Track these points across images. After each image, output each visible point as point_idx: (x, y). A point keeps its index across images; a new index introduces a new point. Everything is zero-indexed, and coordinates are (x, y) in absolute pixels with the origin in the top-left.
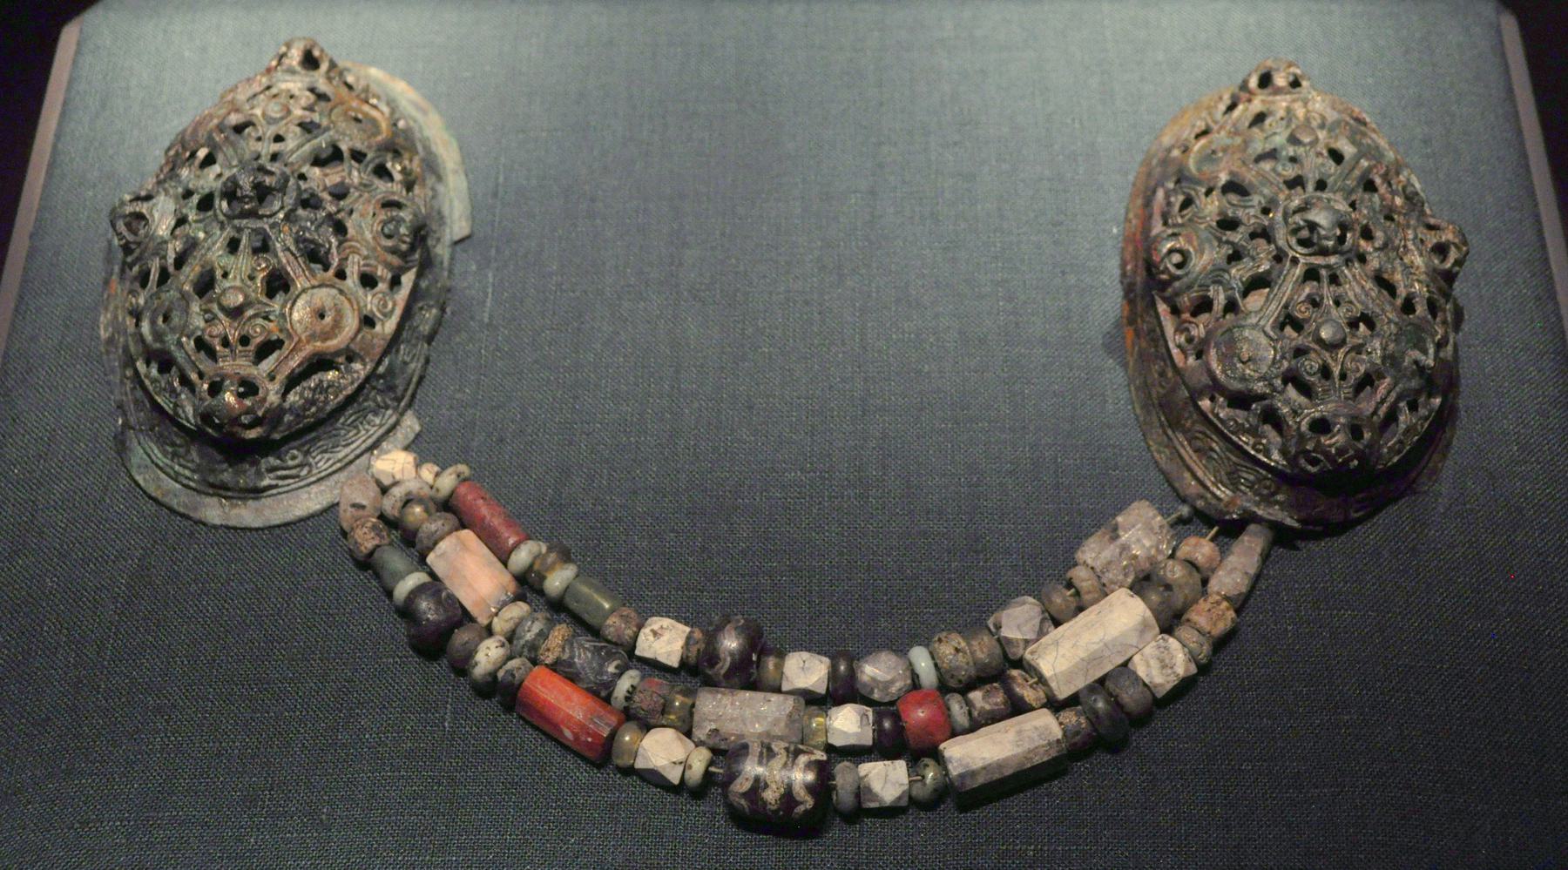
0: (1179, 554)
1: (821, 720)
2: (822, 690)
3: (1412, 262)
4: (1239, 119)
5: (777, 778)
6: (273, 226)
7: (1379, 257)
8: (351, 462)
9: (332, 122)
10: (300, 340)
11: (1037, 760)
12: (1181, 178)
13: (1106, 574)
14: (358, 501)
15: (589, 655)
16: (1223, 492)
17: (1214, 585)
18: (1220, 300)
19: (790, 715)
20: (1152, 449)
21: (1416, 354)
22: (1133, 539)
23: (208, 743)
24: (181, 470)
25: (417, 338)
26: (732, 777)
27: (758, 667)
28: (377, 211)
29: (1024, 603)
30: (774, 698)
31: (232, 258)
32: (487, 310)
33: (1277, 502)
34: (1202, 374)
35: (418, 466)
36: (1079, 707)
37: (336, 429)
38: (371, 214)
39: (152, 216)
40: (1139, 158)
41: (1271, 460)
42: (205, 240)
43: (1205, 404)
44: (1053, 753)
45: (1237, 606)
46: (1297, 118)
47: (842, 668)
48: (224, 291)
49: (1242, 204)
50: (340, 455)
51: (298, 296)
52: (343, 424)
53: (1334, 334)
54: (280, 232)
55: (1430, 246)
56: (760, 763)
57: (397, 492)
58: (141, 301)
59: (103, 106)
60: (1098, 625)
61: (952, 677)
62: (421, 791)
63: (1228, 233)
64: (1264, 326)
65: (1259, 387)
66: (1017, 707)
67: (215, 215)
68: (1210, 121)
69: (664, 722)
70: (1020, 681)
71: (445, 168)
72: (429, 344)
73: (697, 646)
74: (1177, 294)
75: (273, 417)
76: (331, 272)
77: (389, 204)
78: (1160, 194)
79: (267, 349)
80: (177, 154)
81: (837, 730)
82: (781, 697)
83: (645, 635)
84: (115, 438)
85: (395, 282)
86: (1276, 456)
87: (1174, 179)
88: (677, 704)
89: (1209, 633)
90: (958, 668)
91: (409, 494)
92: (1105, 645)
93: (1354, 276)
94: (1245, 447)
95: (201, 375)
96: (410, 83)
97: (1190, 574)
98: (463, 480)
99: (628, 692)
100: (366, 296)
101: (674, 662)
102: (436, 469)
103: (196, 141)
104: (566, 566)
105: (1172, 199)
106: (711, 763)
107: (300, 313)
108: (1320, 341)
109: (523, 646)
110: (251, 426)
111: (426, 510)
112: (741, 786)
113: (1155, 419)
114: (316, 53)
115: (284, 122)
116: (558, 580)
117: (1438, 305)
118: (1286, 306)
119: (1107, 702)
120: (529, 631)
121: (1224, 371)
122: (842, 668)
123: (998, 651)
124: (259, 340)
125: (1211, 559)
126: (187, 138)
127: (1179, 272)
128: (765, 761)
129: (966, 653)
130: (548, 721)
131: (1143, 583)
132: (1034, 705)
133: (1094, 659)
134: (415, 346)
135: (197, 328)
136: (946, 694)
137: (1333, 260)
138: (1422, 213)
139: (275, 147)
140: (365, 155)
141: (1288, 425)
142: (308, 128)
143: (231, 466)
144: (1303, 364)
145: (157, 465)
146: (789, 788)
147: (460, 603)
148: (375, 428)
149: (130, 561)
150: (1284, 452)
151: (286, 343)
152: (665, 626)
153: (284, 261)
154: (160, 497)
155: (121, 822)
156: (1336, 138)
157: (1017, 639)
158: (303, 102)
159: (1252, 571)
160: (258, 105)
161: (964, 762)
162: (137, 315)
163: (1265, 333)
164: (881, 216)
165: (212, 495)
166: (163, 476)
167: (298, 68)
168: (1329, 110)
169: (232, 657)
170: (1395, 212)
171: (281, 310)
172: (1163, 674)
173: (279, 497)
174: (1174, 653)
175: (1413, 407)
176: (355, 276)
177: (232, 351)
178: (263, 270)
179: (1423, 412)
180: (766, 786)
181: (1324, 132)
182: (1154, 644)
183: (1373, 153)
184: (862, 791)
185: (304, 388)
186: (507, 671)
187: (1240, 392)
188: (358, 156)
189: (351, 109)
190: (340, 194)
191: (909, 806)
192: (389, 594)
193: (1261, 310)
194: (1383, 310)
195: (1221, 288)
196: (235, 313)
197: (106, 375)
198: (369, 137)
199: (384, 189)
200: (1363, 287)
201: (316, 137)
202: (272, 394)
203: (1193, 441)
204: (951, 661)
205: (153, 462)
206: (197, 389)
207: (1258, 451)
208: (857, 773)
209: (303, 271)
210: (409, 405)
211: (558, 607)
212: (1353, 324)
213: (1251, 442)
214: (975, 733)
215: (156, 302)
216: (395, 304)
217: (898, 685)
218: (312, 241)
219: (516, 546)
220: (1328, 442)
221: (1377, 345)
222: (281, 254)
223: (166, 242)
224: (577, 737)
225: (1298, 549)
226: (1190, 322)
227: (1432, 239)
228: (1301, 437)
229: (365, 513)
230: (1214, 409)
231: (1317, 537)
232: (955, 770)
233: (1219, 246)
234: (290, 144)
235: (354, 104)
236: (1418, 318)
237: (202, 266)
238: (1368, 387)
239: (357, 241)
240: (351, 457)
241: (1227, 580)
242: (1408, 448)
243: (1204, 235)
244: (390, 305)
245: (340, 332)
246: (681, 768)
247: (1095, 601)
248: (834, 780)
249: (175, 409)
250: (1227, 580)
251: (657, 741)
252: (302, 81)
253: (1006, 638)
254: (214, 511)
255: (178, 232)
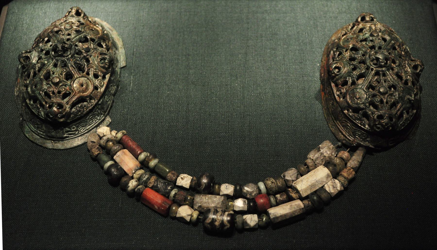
0: (338, 156)
1: (232, 203)
2: (232, 194)
3: (407, 70)
4: (355, 30)
5: (219, 218)
6: (67, 59)
7: (397, 68)
8: (91, 130)
9: (85, 30)
10: (76, 93)
11: (296, 214)
12: (338, 47)
13: (317, 161)
14: (93, 140)
15: (163, 184)
16: (351, 138)
17: (349, 164)
18: (350, 81)
19: (222, 201)
20: (330, 127)
21: (408, 97)
22: (324, 151)
23: (48, 211)
24: (40, 132)
25: (110, 94)
26: (206, 218)
27: (213, 188)
28: (99, 56)
29: (292, 170)
30: (218, 197)
31: (56, 69)
32: (131, 87)
33: (367, 141)
34: (345, 103)
35: (111, 131)
36: (309, 199)
37: (86, 120)
38: (97, 56)
39: (31, 57)
40: (325, 44)
41: (366, 128)
42: (47, 63)
43: (346, 112)
44: (301, 212)
45: (356, 171)
46: (373, 30)
47: (238, 188)
48: (53, 78)
49: (357, 53)
50: (87, 128)
51: (75, 80)
52: (88, 118)
53: (384, 90)
54: (70, 61)
55: (412, 66)
56: (214, 214)
57: (105, 138)
58: (28, 82)
59: (15, 29)
60: (314, 176)
61: (271, 190)
62: (112, 224)
63: (352, 62)
64: (363, 88)
65: (362, 106)
66: (290, 199)
67: (50, 56)
68: (346, 31)
69: (185, 204)
70: (291, 191)
71: (118, 46)
72: (114, 97)
73: (195, 182)
74: (337, 80)
75: (68, 115)
76: (85, 73)
77: (101, 54)
78: (332, 52)
79: (65, 96)
80: (38, 40)
81: (237, 206)
82: (220, 196)
83: (179, 178)
84: (19, 124)
85: (104, 78)
86: (367, 126)
87: (336, 48)
88: (189, 198)
89: (347, 178)
90: (272, 188)
91: (108, 138)
92: (316, 181)
93: (390, 74)
94: (358, 124)
95: (46, 103)
96: (108, 23)
97: (341, 161)
98: (124, 135)
99: (174, 195)
100: (95, 80)
101: (187, 186)
102: (116, 132)
103: (44, 36)
104: (155, 159)
105: (336, 53)
106: (199, 215)
107: (75, 85)
108: (380, 92)
109: (143, 182)
110: (61, 118)
111: (113, 143)
112: (208, 221)
113: (331, 118)
114: (80, 11)
115: (70, 30)
116: (153, 163)
117: (415, 83)
118: (370, 82)
119: (317, 197)
120: (144, 178)
121: (351, 102)
122: (238, 188)
123: (284, 183)
124: (64, 92)
125: (348, 157)
126: (41, 35)
127: (338, 73)
128: (215, 214)
129: (275, 183)
130: (150, 203)
131: (328, 164)
132: (295, 198)
133: (313, 185)
134: (110, 97)
135: (45, 89)
136: (269, 195)
137: (384, 69)
138: (410, 57)
139: (68, 37)
140: (95, 40)
141: (371, 117)
142: (78, 32)
143: (55, 130)
144: (375, 99)
145: (33, 131)
146: (223, 221)
147: (123, 170)
148: (98, 120)
149: (24, 159)
150: (369, 125)
151: (71, 94)
152: (185, 176)
153: (71, 69)
154: (33, 140)
155: (22, 233)
156: (384, 35)
157: (290, 180)
158: (76, 25)
159: (360, 161)
160: (63, 26)
161: (275, 214)
162: (26, 86)
163: (363, 90)
164: (248, 60)
165: (49, 140)
166: (34, 134)
167: (75, 15)
168: (382, 27)
169: (55, 186)
170: (402, 56)
171: (70, 83)
172: (334, 190)
173: (69, 140)
174: (337, 184)
175: (408, 113)
176: (92, 74)
177: (55, 96)
178: (65, 72)
179: (411, 114)
180: (216, 221)
181: (381, 33)
182: (331, 181)
183: (396, 40)
184: (244, 223)
185: (77, 107)
186: (138, 189)
187: (356, 108)
188: (93, 40)
189: (91, 27)
190: (88, 50)
191: (258, 227)
192: (102, 167)
193: (362, 84)
194: (399, 84)
195: (350, 77)
196: (56, 84)
197: (17, 106)
198: (96, 35)
199: (100, 50)
200: (393, 77)
201: (80, 34)
202: (67, 108)
203: (342, 124)
204: (270, 186)
205: (31, 130)
206: (45, 107)
207: (362, 125)
208: (243, 218)
209: (77, 72)
210: (108, 114)
211: (153, 171)
212: (390, 88)
213: (359, 123)
214: (278, 206)
215: (32, 82)
216: (104, 83)
217: (255, 193)
218: (79, 64)
219: (140, 153)
220: (382, 121)
221: (397, 93)
222: (70, 67)
223: (35, 65)
224: (159, 208)
225: (373, 155)
226: (341, 88)
227: (413, 64)
228: (375, 120)
229: (95, 144)
230: (348, 113)
231: (379, 151)
232: (272, 217)
233: (350, 66)
234: (73, 36)
235: (91, 26)
236: (409, 86)
237: (46, 71)
238: (394, 107)
239: (93, 64)
240: (91, 128)
241: (353, 163)
242: (406, 124)
243: (345, 62)
244: (102, 84)
245: (88, 91)
246: (190, 217)
247: (313, 169)
248: (236, 220)
249: (38, 113)
250: (353, 163)
251: (183, 209)
252: (75, 19)
253: (287, 180)
254: (49, 145)
255: (39, 61)
